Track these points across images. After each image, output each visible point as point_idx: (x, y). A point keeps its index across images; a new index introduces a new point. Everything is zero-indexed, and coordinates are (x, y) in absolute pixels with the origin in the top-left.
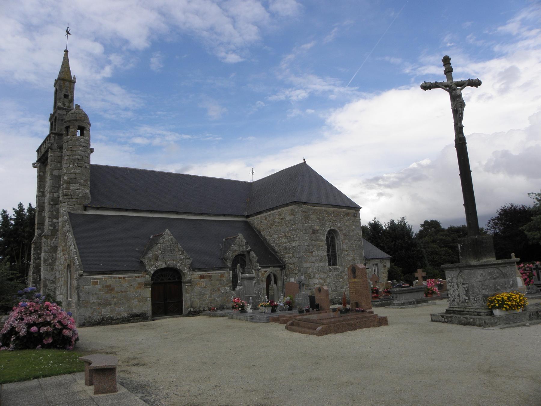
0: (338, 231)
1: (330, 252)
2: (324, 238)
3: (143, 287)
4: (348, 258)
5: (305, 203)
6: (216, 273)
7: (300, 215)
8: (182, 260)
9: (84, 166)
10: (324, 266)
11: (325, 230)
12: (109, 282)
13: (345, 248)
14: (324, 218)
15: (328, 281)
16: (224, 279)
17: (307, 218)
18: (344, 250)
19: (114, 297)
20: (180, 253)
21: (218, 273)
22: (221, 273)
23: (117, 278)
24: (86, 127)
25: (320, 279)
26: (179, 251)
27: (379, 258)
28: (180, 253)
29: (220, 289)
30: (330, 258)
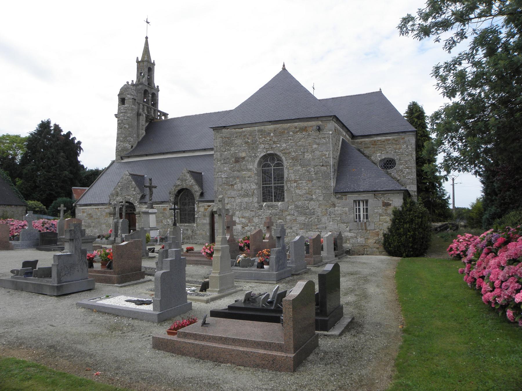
0: (281, 155)
1: (272, 183)
2: (254, 166)
3: (109, 216)
4: (298, 191)
5: (224, 127)
6: (160, 207)
7: (218, 143)
8: (134, 195)
9: (123, 127)
10: (251, 202)
11: (256, 157)
12: (90, 212)
13: (293, 177)
14: (255, 140)
15: (256, 222)
16: (167, 212)
17: (228, 144)
18: (290, 181)
19: (92, 222)
20: (133, 189)
21: (162, 207)
22: (164, 207)
23: (94, 209)
24: (125, 97)
25: (243, 218)
26: (132, 188)
27: (372, 191)
28: (133, 189)
29: (163, 221)
30: (272, 192)
